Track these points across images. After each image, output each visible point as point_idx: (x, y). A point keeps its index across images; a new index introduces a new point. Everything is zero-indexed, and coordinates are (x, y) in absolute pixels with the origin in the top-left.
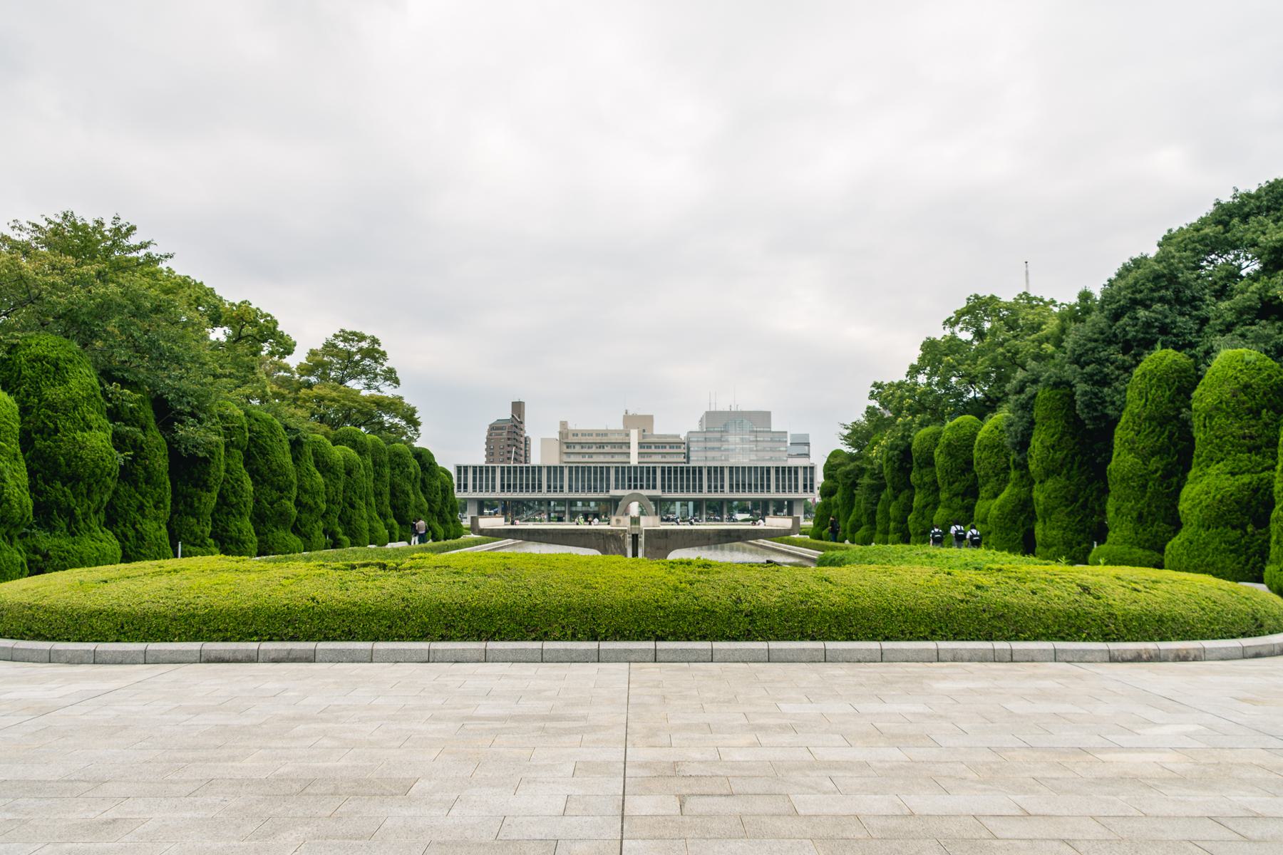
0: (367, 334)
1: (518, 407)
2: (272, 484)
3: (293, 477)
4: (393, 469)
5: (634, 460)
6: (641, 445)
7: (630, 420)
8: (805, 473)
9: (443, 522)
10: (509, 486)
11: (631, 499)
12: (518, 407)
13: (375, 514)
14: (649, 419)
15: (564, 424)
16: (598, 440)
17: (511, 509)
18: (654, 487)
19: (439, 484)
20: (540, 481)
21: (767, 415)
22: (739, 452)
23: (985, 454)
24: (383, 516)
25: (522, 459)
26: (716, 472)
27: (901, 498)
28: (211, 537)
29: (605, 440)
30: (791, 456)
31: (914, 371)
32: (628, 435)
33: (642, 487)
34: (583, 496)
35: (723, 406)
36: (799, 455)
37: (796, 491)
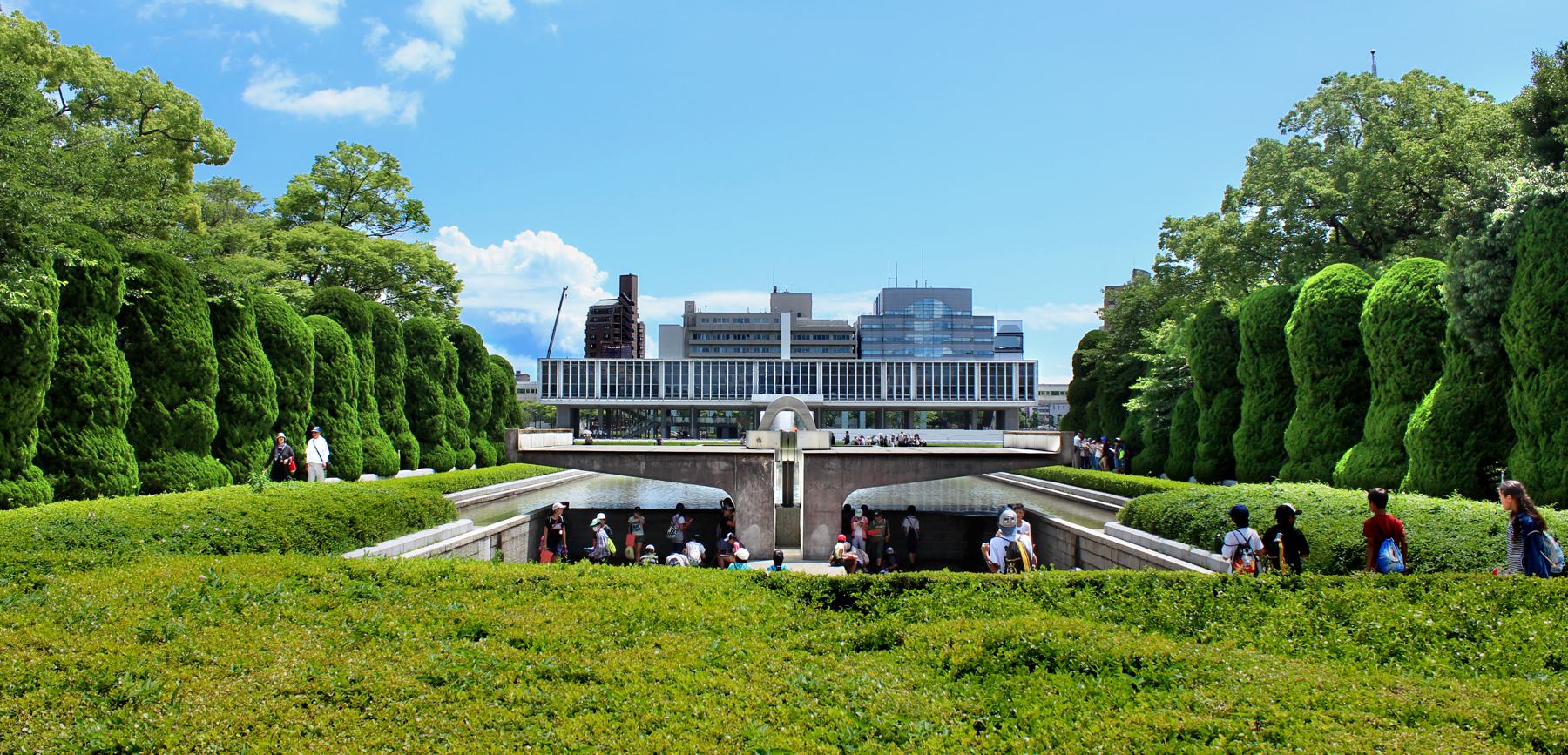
0: (377, 149)
1: (627, 284)
2: (172, 375)
3: (212, 365)
4: (411, 355)
6: (795, 334)
7: (781, 300)
8: (1022, 373)
9: (496, 438)
10: (613, 389)
11: (778, 407)
12: (627, 284)
13: (376, 426)
14: (806, 299)
15: (690, 306)
16: (737, 327)
17: (572, 419)
18: (814, 391)
19: (489, 381)
20: (655, 381)
23: (1387, 326)
24: (391, 428)
25: (634, 352)
27: (1217, 404)
28: (35, 462)
29: (745, 327)
30: (998, 351)
31: (1231, 203)
32: (777, 320)
33: (796, 391)
34: (715, 402)
35: (906, 282)
36: (1008, 350)
37: (1010, 398)
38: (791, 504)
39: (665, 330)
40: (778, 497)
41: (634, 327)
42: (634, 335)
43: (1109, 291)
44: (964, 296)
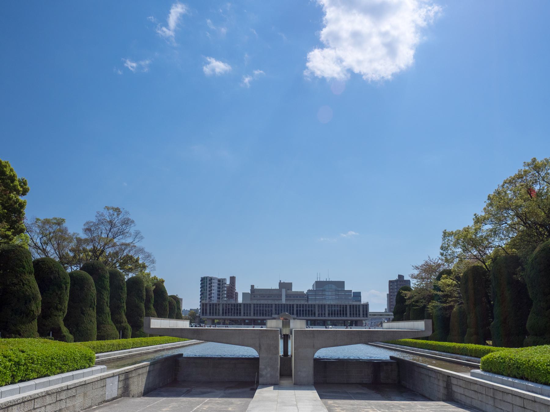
5: (284, 301)
6: (287, 296)
7: (282, 285)
12: (233, 279)
15: (252, 286)
21: (343, 283)
22: (330, 300)
26: (322, 307)
31: (478, 220)
35: (323, 279)
38: (287, 355)
39: (244, 294)
40: (281, 353)
41: (234, 293)
42: (234, 296)
43: (391, 282)
44: (342, 284)
